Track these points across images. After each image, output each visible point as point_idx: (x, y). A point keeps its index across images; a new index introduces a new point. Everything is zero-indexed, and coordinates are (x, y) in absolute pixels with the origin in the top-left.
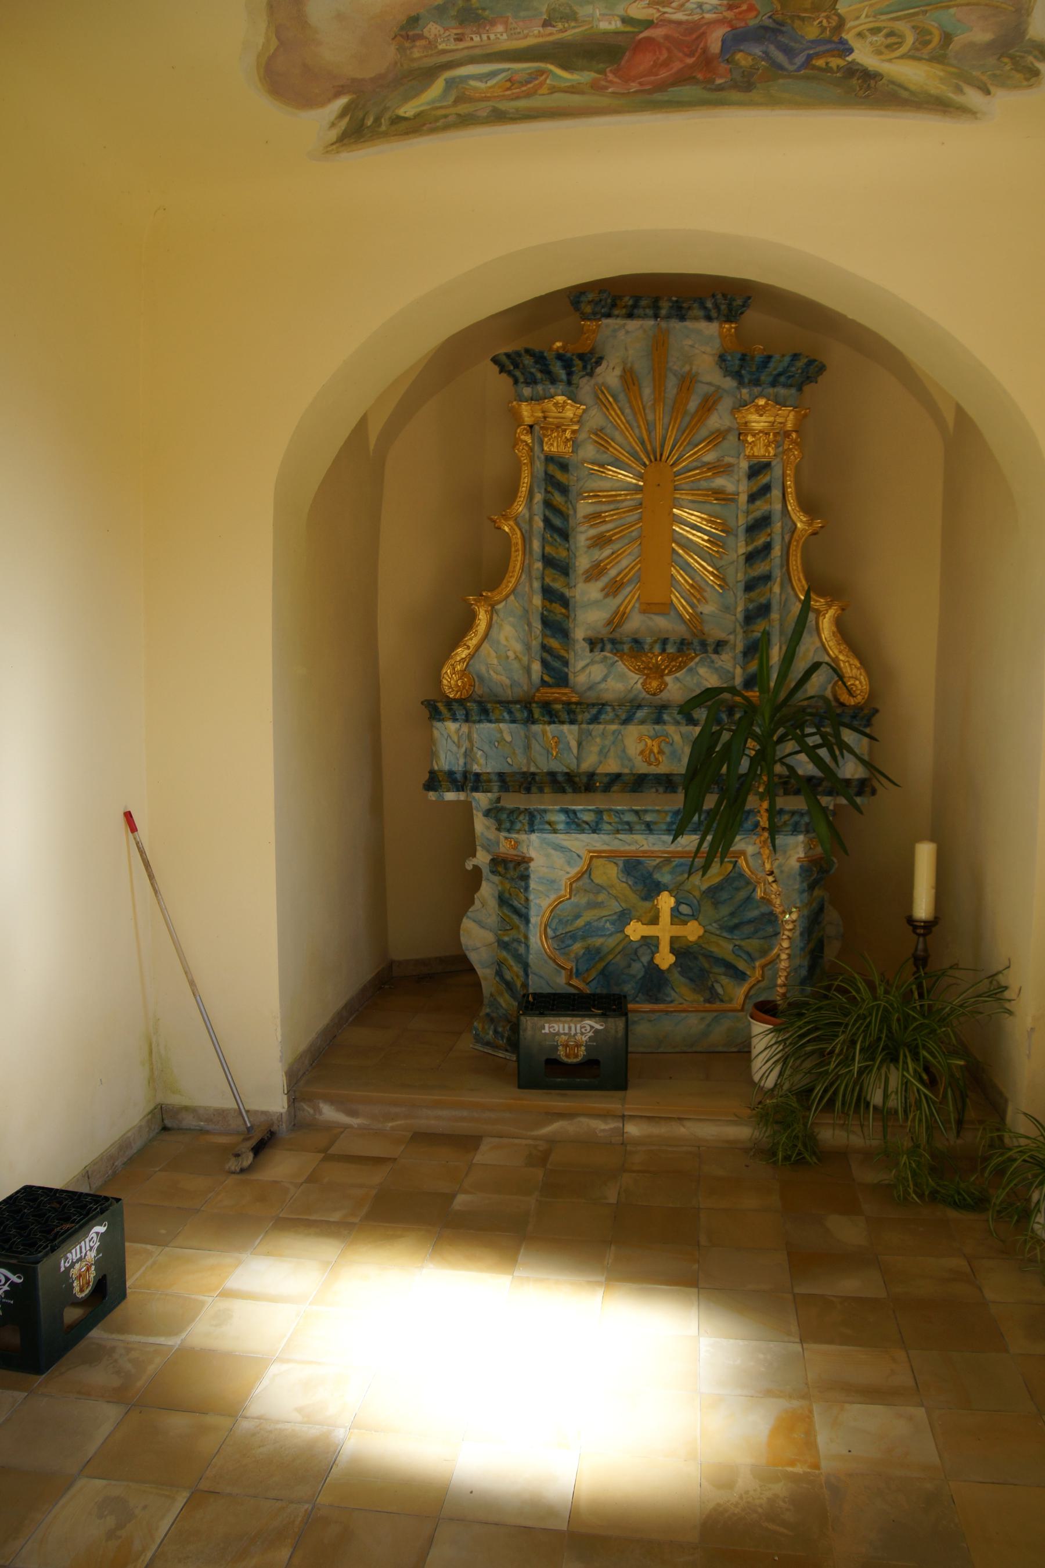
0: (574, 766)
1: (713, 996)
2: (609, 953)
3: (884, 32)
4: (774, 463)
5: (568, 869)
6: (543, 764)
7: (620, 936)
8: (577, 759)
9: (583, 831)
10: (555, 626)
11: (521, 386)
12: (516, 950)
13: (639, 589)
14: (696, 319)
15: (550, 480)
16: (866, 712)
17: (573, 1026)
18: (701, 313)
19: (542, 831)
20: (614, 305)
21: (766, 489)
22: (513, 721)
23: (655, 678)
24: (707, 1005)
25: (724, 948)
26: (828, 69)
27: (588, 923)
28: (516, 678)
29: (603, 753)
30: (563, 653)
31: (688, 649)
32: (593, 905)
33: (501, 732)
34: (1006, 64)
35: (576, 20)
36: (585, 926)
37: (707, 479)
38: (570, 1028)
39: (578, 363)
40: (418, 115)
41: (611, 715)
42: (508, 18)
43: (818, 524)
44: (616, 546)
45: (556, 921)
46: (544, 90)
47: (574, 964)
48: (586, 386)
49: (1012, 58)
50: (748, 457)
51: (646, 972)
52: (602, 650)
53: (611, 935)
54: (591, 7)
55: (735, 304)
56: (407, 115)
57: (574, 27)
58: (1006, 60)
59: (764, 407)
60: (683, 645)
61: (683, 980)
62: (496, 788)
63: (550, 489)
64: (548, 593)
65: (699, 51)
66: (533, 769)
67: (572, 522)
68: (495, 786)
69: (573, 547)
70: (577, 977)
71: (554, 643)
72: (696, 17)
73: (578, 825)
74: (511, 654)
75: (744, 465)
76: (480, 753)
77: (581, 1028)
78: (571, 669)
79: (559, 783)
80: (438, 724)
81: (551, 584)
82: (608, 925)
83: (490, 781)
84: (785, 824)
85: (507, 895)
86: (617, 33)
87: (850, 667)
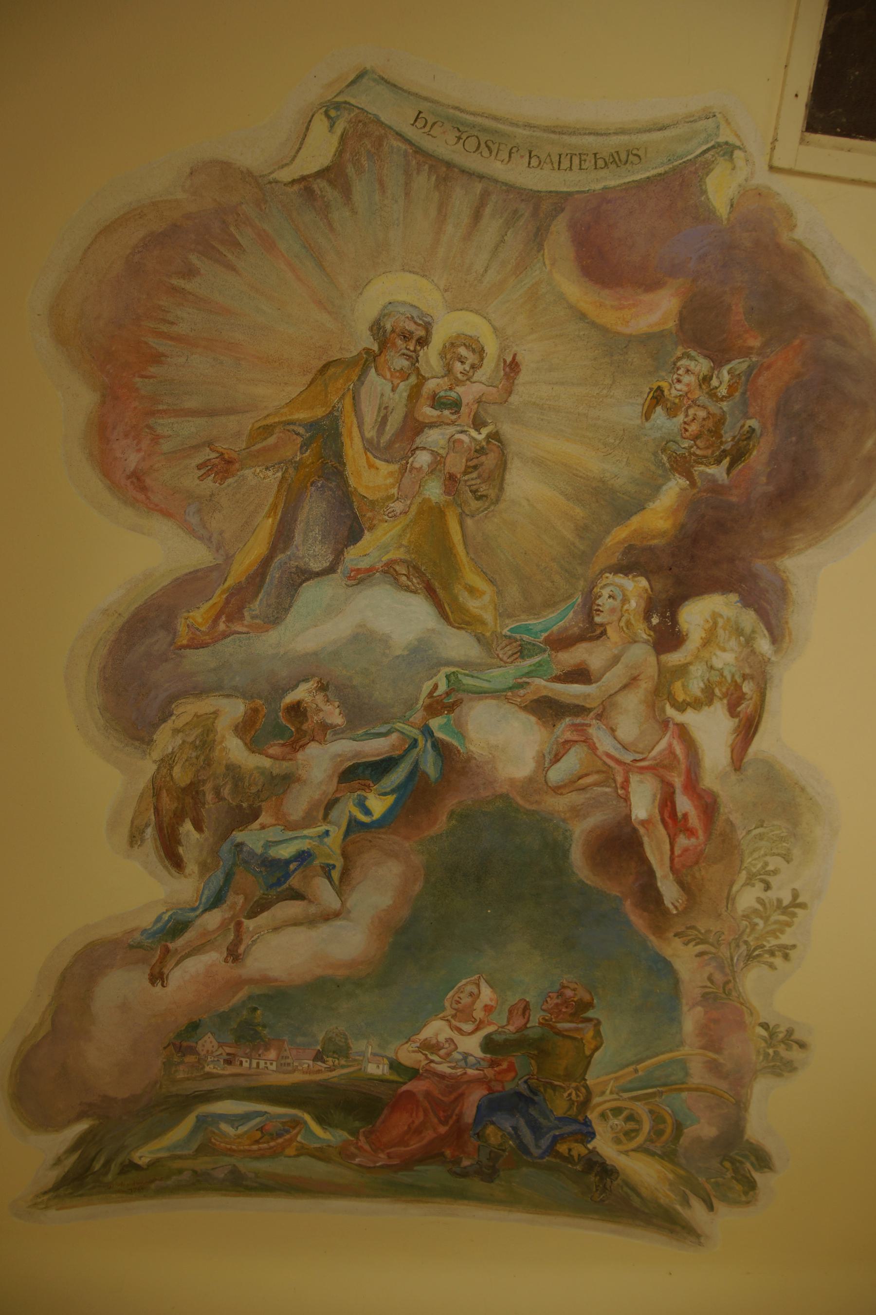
3: (625, 1113)
26: (569, 1159)
34: (728, 1170)
35: (347, 1056)
40: (153, 1164)
42: (284, 1041)
46: (291, 1151)
49: (733, 1162)
54: (365, 1042)
56: (140, 1163)
57: (343, 1067)
58: (727, 1164)
65: (454, 1117)
72: (459, 1072)
86: (382, 1081)
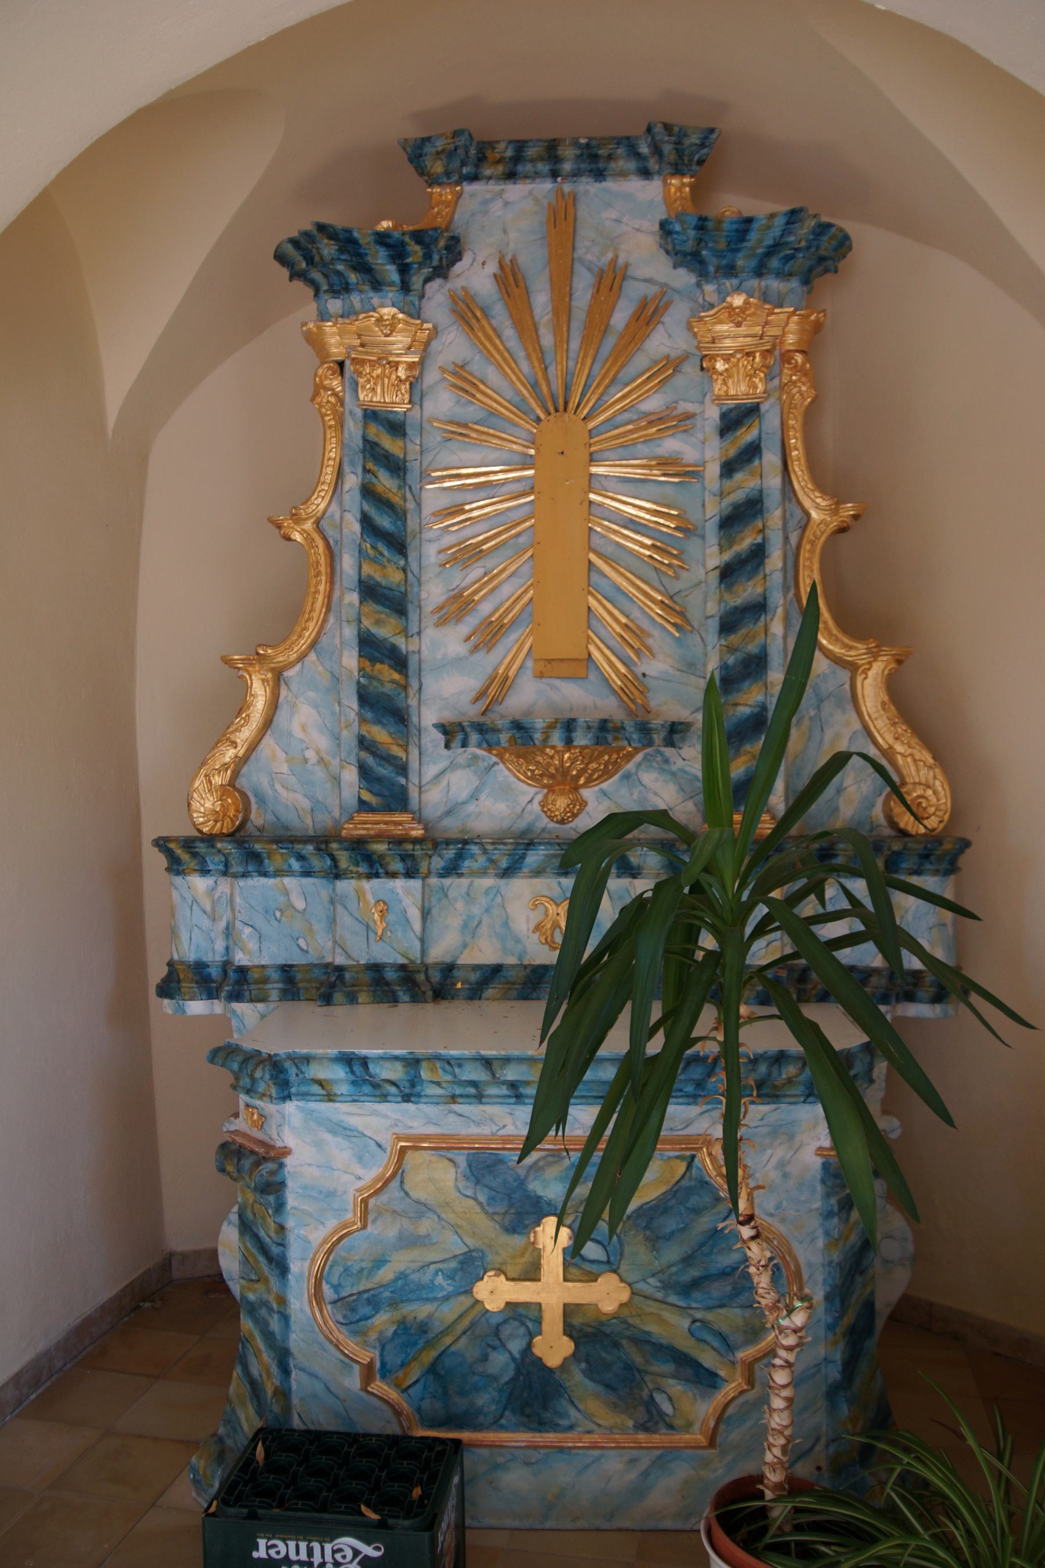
0: (415, 954)
1: (652, 1420)
2: (444, 1333)
4: (764, 408)
5: (360, 1171)
6: (360, 951)
7: (465, 1301)
8: (422, 940)
9: (384, 1098)
10: (384, 700)
11: (325, 297)
12: (267, 1324)
13: (531, 632)
14: (623, 174)
15: (372, 450)
16: (947, 846)
17: (316, 1546)
18: (632, 165)
19: (304, 1096)
20: (481, 159)
21: (753, 451)
22: (307, 873)
23: (562, 793)
24: (642, 1436)
25: (673, 1326)
27: (402, 1276)
28: (320, 795)
29: (470, 929)
30: (397, 751)
31: (616, 739)
32: (410, 1241)
33: (286, 893)
36: (397, 1279)
37: (648, 440)
38: (310, 1552)
39: (415, 251)
41: (482, 860)
43: (848, 510)
44: (489, 562)
45: (338, 1270)
47: (377, 1353)
48: (437, 297)
50: (719, 398)
51: (518, 1371)
52: (464, 744)
53: (447, 1298)
55: (687, 142)
59: (743, 309)
60: (604, 729)
61: (590, 1385)
62: (274, 995)
63: (370, 465)
64: (369, 646)
66: (340, 960)
67: (412, 523)
68: (274, 990)
69: (414, 566)
70: (383, 1377)
71: (380, 734)
73: (376, 1086)
74: (310, 754)
75: (713, 414)
76: (248, 930)
77: (334, 1552)
78: (414, 778)
79: (387, 984)
80: (178, 880)
81: (374, 630)
82: (440, 1279)
83: (265, 980)
84: (790, 1081)
85: (250, 1215)
87: (915, 765)
